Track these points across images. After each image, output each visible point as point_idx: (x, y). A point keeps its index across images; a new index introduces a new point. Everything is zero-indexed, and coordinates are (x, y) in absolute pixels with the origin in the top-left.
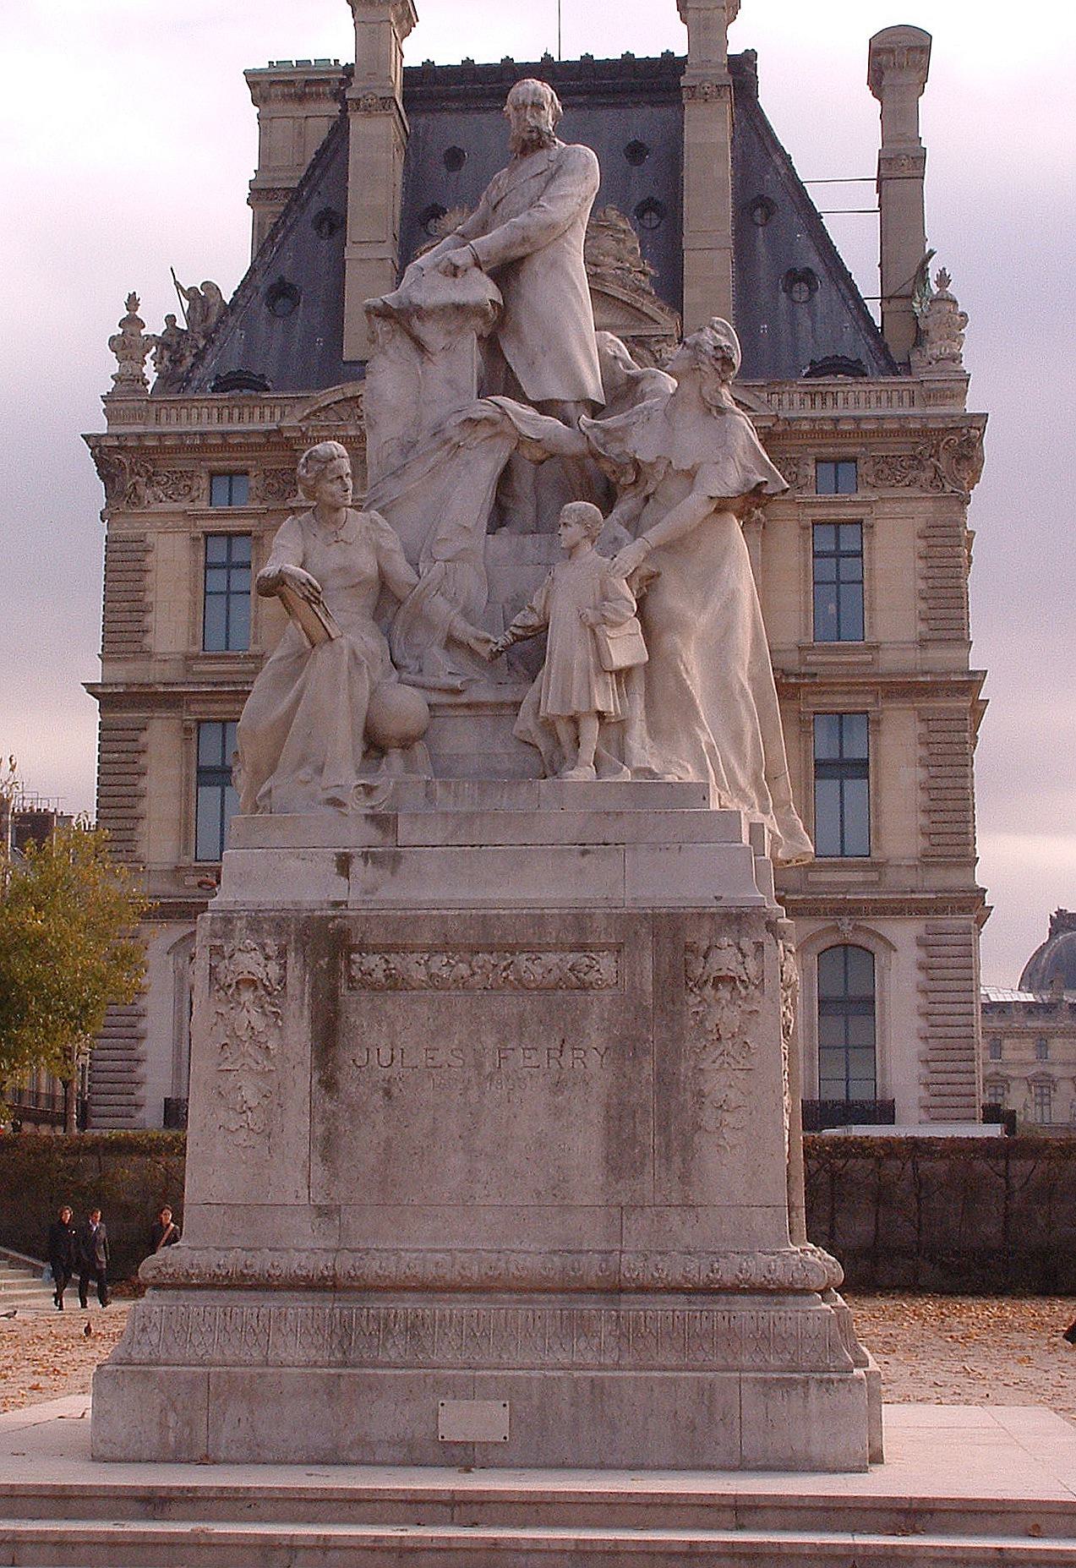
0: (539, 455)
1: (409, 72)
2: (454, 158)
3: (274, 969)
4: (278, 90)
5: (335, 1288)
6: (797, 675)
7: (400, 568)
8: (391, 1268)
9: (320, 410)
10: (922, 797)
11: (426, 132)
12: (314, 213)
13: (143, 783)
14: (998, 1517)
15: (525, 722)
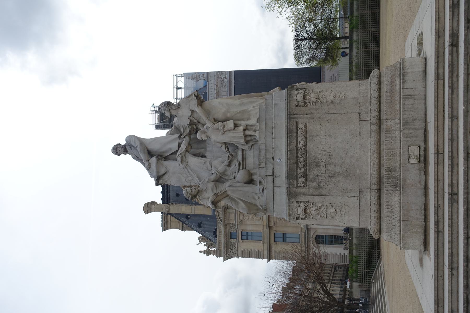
0: (190, 147)
2: (177, 195)
3: (302, 205)
5: (380, 190)
7: (213, 177)
8: (375, 174)
14: (440, 13)
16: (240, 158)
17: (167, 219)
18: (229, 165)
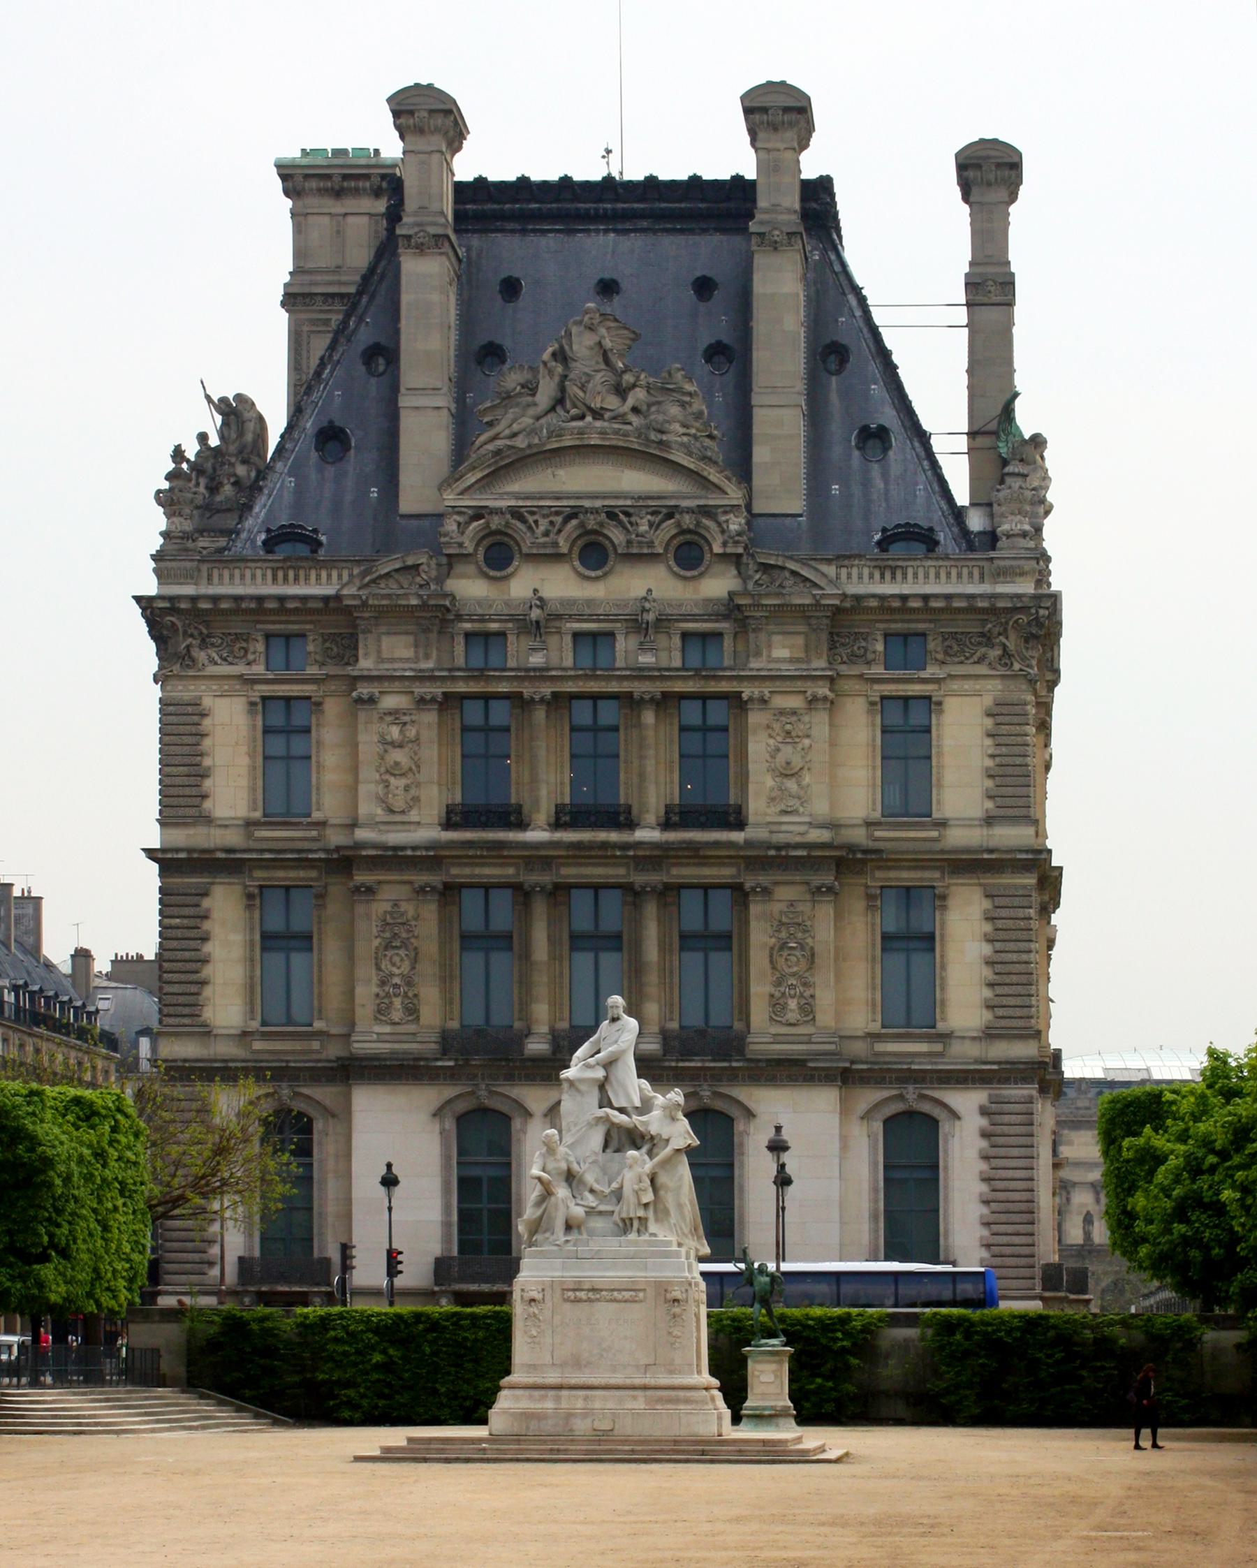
1: (460, 187)
2: (511, 288)
4: (313, 184)
6: (865, 852)
7: (575, 1167)
9: (381, 577)
10: (987, 973)
11: (479, 255)
12: (362, 347)
13: (207, 948)
15: (616, 1217)
16: (602, 1208)
17: (356, 192)
18: (592, 1191)
